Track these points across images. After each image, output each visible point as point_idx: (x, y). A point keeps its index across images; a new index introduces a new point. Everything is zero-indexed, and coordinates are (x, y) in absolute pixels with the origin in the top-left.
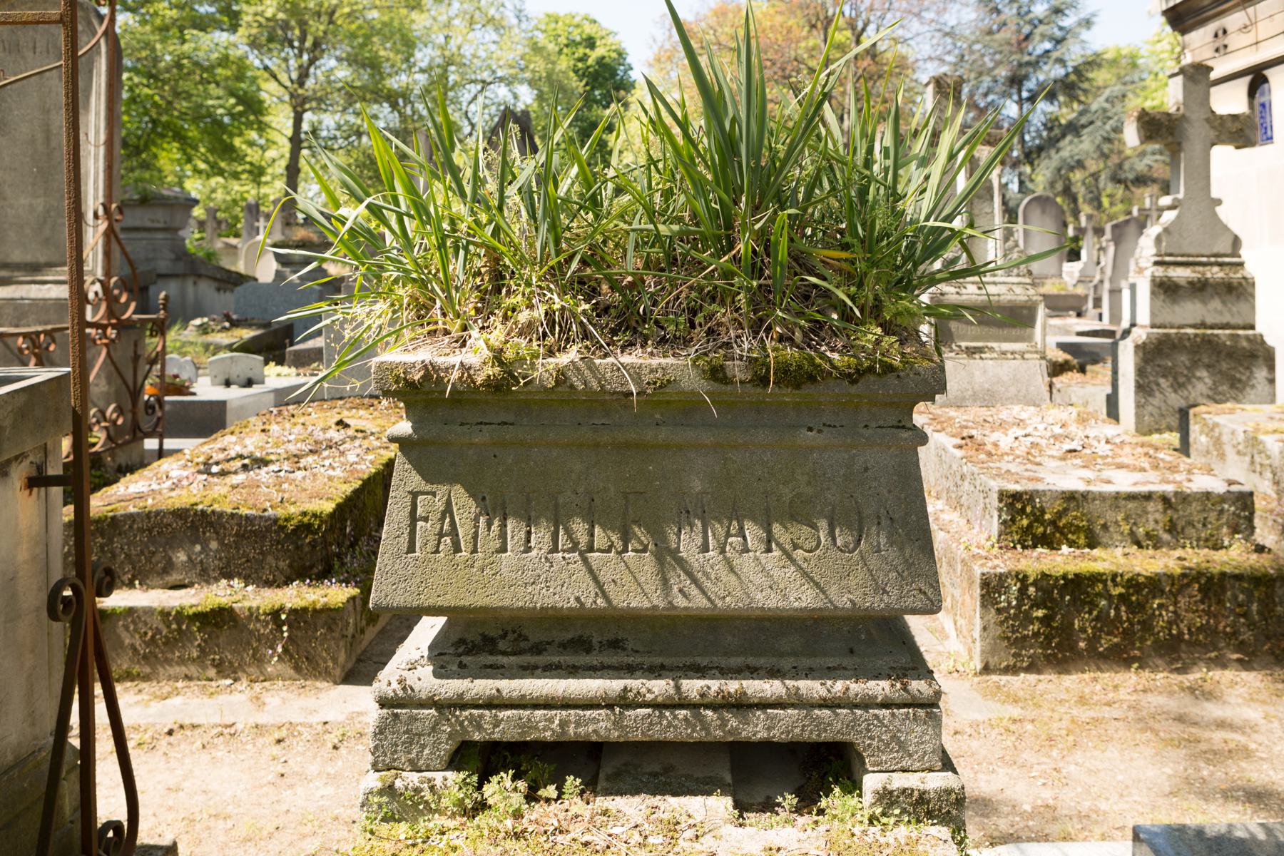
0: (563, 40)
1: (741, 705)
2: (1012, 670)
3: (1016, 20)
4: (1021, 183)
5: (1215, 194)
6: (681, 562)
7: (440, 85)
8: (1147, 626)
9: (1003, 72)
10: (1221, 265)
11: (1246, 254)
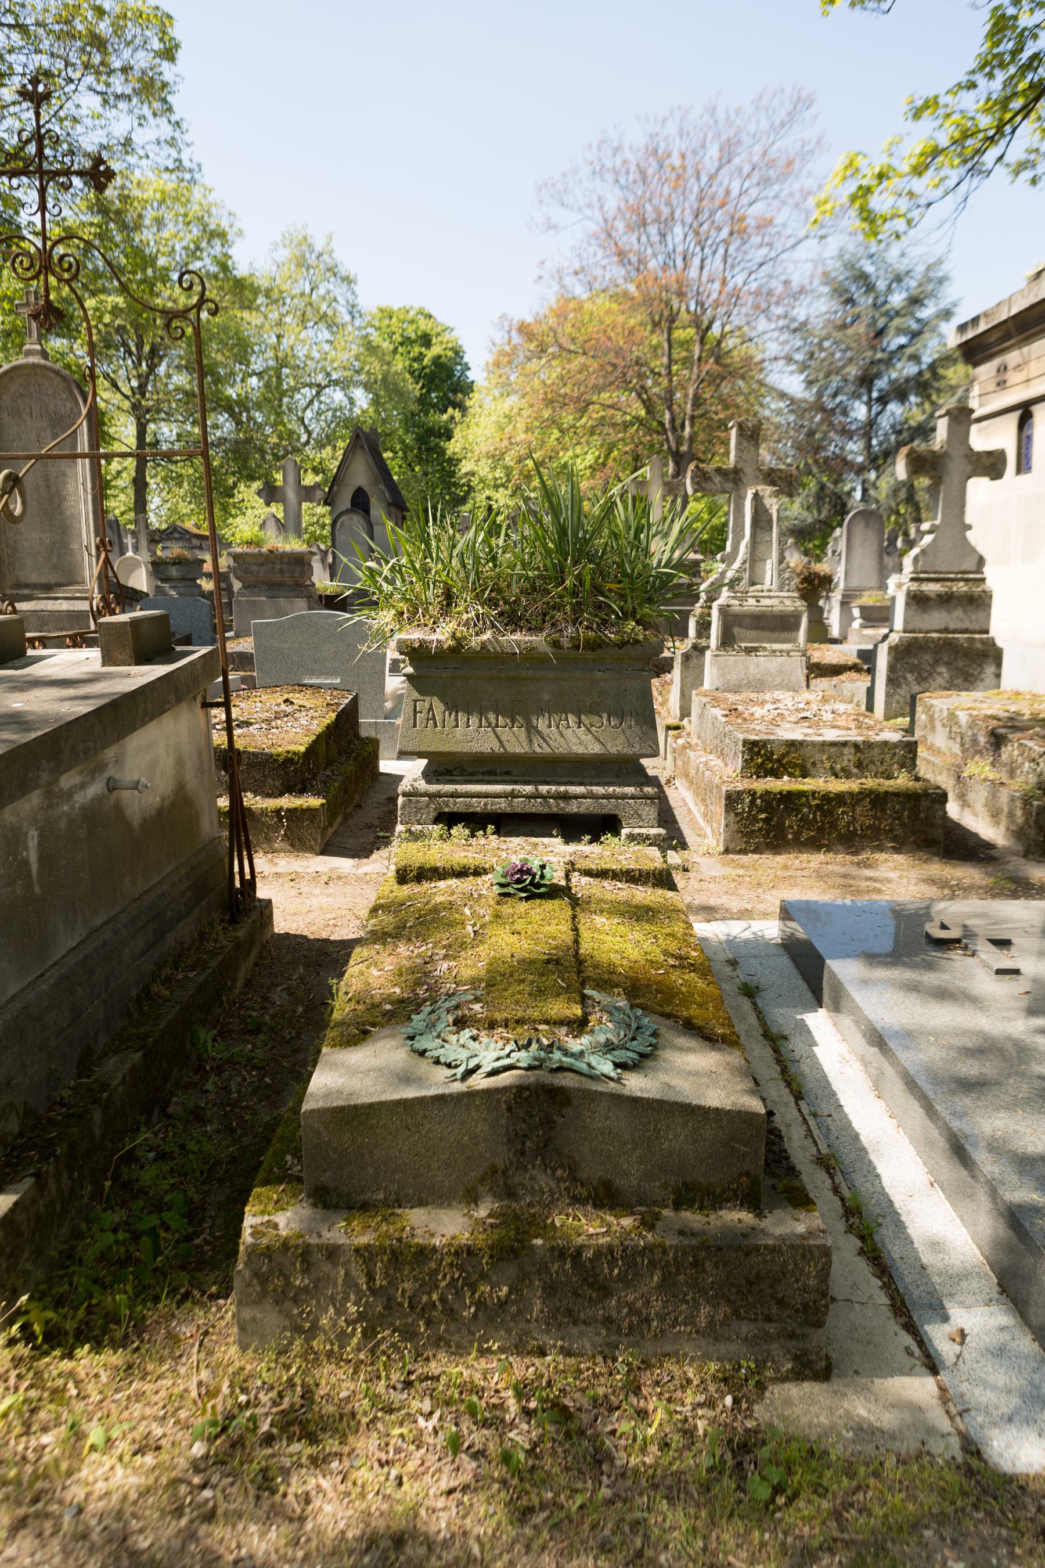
0: (397, 338)
1: (566, 797)
2: (743, 852)
3: (871, 312)
4: (865, 491)
5: (968, 519)
6: (539, 732)
7: (275, 394)
8: (833, 825)
9: (853, 371)
10: (966, 580)
11: (988, 571)
